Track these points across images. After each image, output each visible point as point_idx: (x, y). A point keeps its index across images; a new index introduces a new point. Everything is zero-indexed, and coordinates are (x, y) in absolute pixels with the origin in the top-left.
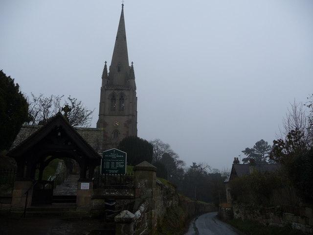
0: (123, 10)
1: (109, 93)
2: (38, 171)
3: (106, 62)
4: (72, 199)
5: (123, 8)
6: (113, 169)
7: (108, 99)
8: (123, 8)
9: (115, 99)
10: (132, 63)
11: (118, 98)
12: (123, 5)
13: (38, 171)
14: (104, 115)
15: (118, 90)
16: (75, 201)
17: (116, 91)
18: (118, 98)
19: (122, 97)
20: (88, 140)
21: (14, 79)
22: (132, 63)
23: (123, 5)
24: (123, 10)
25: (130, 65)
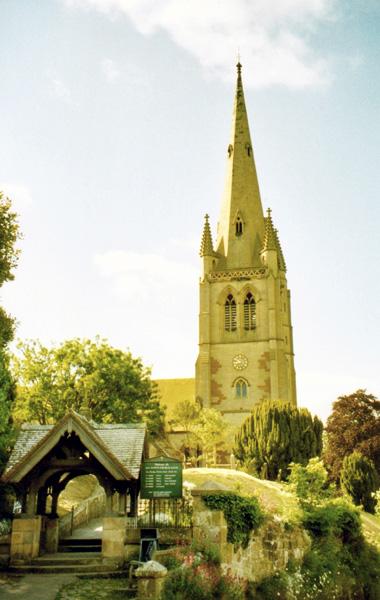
0: (239, 79)
1: (219, 288)
2: (50, 498)
3: (207, 217)
4: (96, 545)
5: (239, 72)
6: (161, 490)
7: (218, 303)
8: (239, 72)
9: (234, 303)
10: (269, 211)
11: (239, 299)
12: (239, 66)
13: (50, 498)
14: (211, 344)
15: (240, 280)
16: (99, 550)
17: (234, 284)
18: (239, 299)
19: (249, 295)
20: (109, 446)
21: (12, 278)
22: (269, 211)
23: (239, 66)
24: (239, 79)
25: (266, 215)
